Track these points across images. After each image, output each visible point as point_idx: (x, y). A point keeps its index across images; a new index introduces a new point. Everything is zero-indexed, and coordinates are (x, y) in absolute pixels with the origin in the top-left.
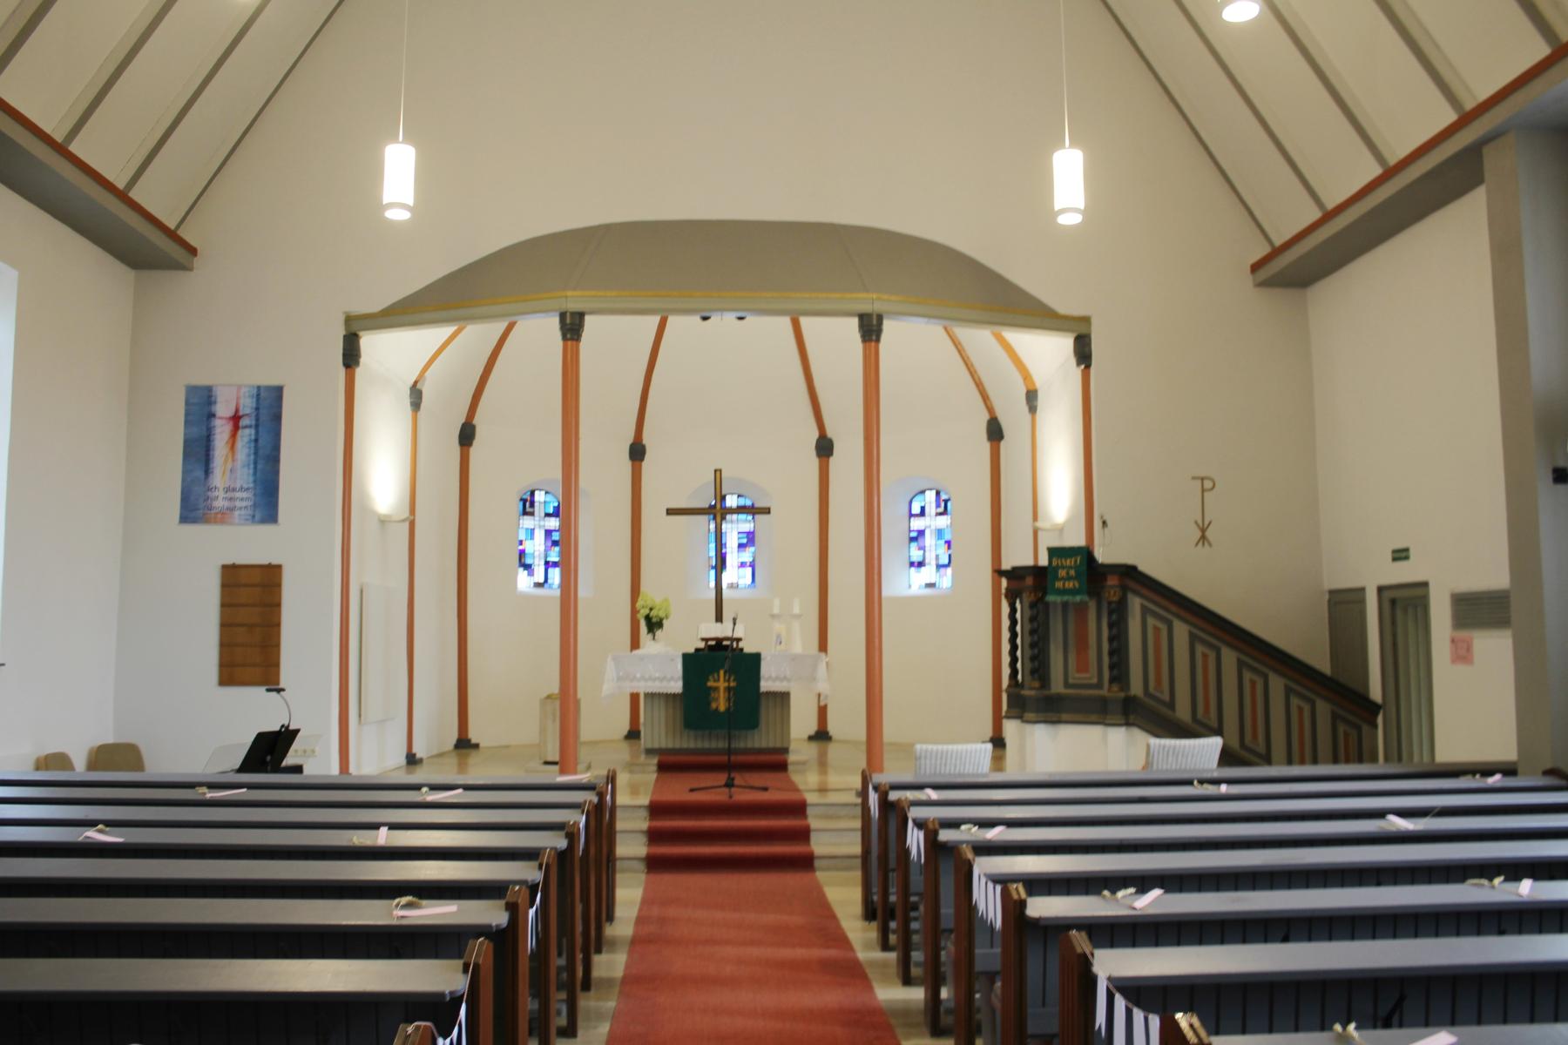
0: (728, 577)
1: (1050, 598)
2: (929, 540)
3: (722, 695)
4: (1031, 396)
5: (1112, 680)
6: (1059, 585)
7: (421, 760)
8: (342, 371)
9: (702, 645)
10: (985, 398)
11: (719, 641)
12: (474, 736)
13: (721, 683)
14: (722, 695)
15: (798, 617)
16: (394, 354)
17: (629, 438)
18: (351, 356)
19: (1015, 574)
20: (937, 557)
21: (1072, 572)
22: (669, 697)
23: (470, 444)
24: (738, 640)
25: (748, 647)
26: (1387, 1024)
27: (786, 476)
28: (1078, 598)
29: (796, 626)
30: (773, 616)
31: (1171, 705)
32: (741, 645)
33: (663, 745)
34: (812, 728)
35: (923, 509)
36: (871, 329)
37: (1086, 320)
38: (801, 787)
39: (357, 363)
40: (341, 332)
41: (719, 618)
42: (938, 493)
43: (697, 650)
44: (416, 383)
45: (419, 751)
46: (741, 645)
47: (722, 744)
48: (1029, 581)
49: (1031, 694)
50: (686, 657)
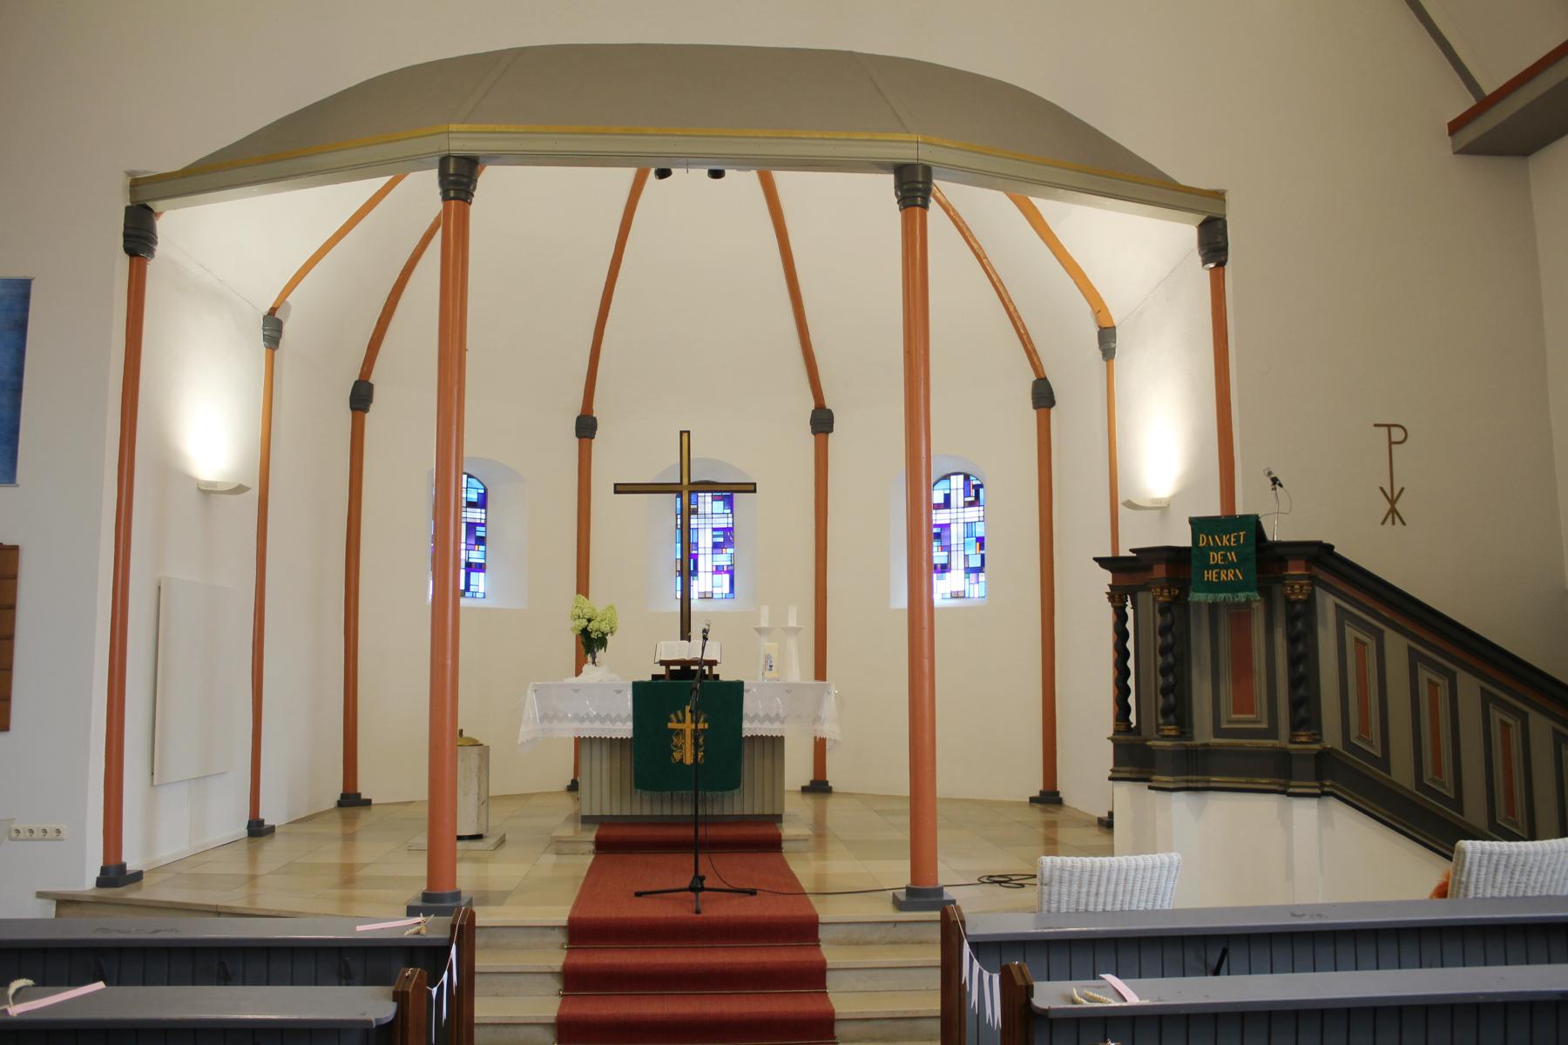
0: (699, 585)
1: (1196, 597)
2: (956, 532)
3: (688, 754)
4: (1106, 337)
5: (1297, 725)
6: (1211, 575)
7: (272, 829)
8: (123, 260)
9: (662, 670)
10: (1031, 354)
11: (685, 664)
12: (364, 790)
13: (686, 725)
14: (688, 754)
15: (796, 631)
16: (190, 230)
17: (577, 410)
18: (139, 237)
19: (1145, 558)
20: (966, 557)
21: (1232, 556)
22: (613, 743)
23: (366, 410)
24: (712, 663)
25: (725, 674)
26: (1216, 972)
27: (772, 449)
28: (1241, 597)
29: (792, 644)
30: (759, 631)
31: (1384, 762)
32: (716, 670)
33: (607, 813)
34: (807, 777)
35: (947, 497)
36: (913, 188)
37: (1219, 196)
38: (807, 884)
39: (150, 251)
40: (121, 202)
41: (685, 634)
42: (967, 478)
43: (655, 677)
44: (273, 311)
45: (268, 816)
46: (716, 670)
47: (688, 811)
48: (1160, 571)
49: (1162, 748)
50: (638, 687)
